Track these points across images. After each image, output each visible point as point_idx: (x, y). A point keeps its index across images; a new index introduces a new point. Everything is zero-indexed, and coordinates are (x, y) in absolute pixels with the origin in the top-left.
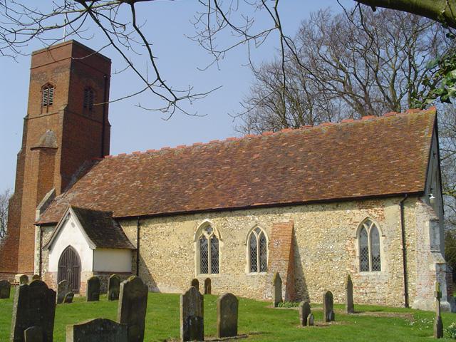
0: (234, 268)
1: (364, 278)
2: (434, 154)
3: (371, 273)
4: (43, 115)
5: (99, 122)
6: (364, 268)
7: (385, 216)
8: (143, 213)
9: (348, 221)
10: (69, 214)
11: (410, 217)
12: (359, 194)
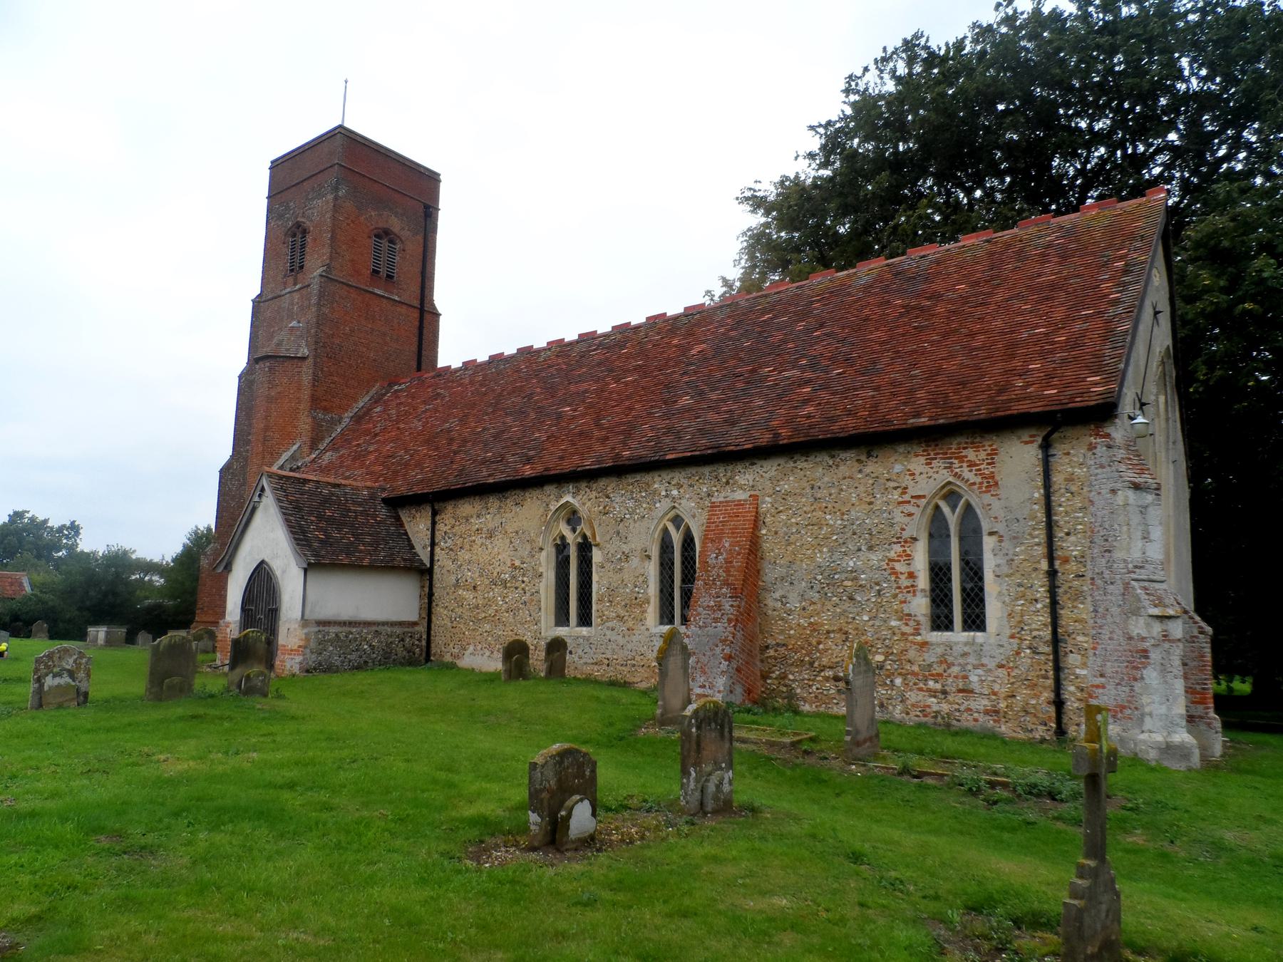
0: (622, 613)
1: (939, 650)
2: (1156, 313)
3: (958, 636)
4: (288, 290)
5: (415, 307)
6: (941, 621)
7: (997, 478)
8: (440, 485)
9: (896, 496)
10: (263, 487)
11: (1070, 479)
12: (923, 421)
